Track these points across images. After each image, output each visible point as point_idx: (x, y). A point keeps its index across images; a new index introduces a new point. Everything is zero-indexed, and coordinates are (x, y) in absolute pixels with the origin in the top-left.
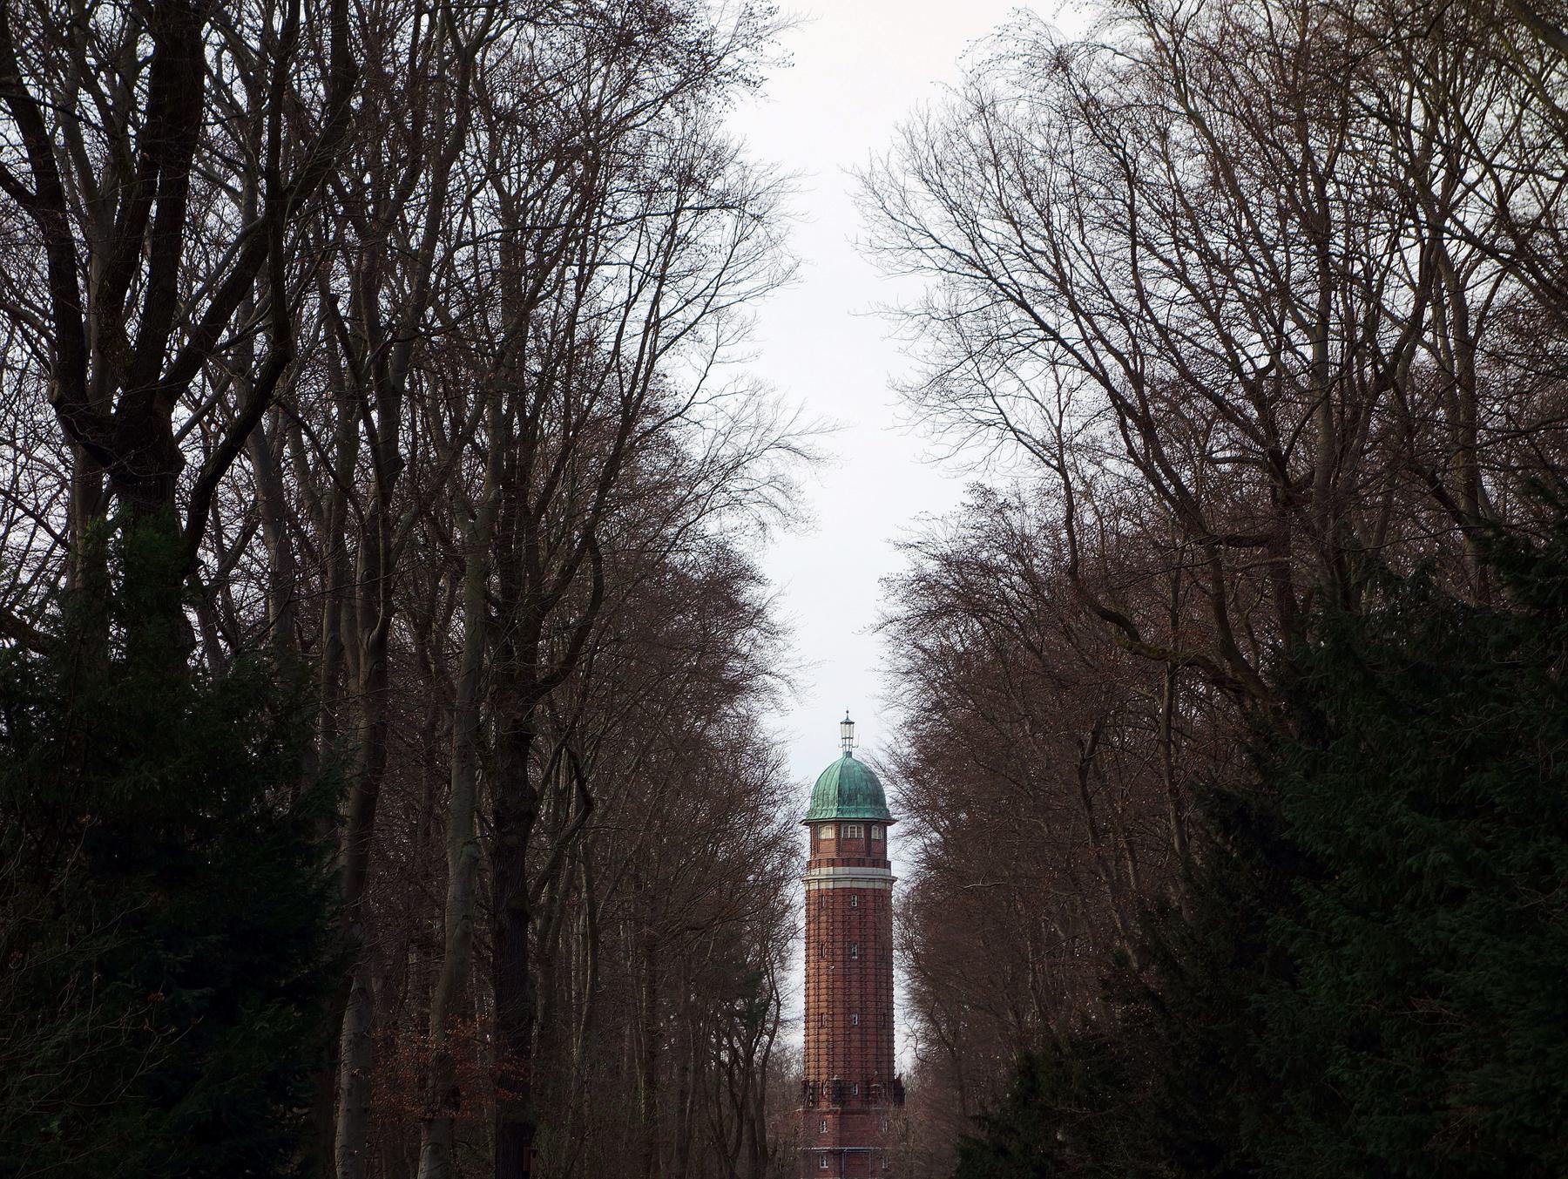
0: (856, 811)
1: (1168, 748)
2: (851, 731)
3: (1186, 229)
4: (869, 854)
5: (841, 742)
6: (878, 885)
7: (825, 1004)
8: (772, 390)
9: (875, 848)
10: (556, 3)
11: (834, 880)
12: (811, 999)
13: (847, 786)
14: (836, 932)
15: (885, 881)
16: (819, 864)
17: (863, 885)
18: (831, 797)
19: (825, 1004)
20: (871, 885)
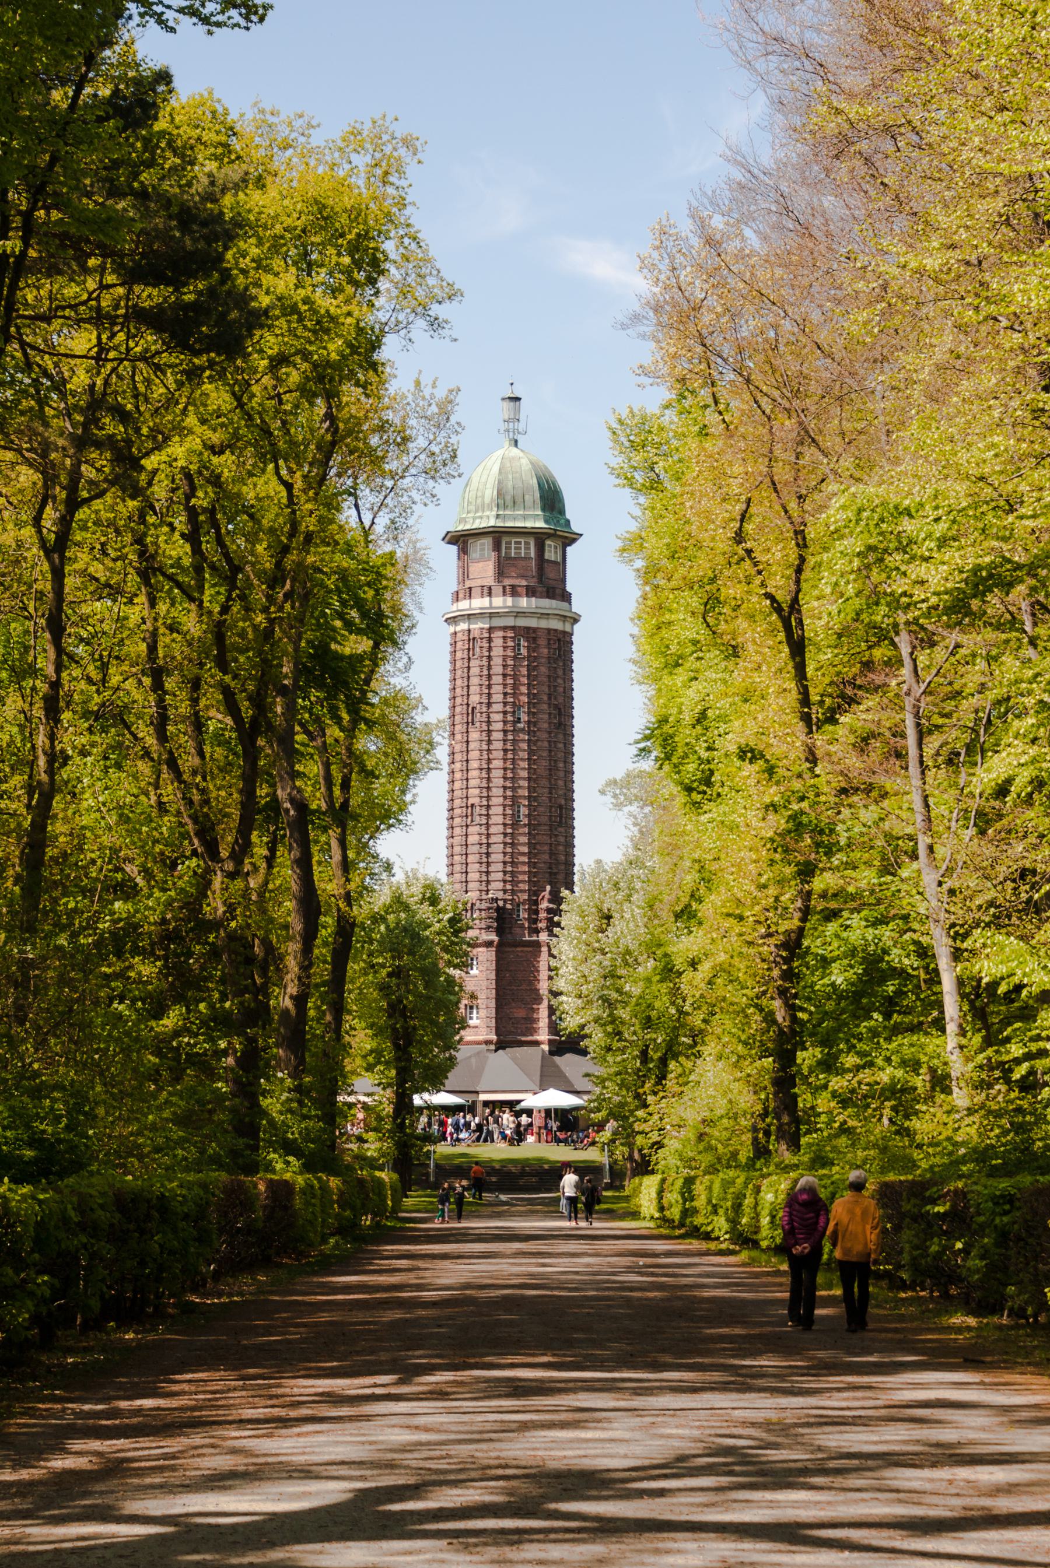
0: (525, 517)
1: (356, 218)
2: (517, 411)
3: (147, 754)
4: (540, 581)
5: (503, 426)
6: (556, 624)
7: (477, 791)
8: (781, 670)
9: (551, 573)
10: (1048, 815)
11: (492, 615)
12: (458, 785)
13: (510, 484)
14: (492, 877)
15: (564, 618)
16: (469, 593)
17: (533, 623)
18: (487, 500)
19: (477, 791)
20: (544, 624)
